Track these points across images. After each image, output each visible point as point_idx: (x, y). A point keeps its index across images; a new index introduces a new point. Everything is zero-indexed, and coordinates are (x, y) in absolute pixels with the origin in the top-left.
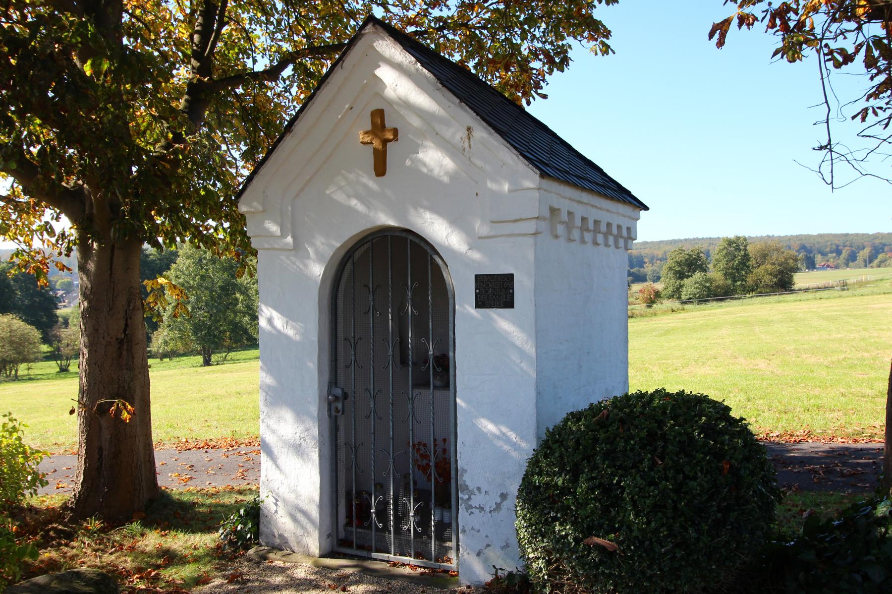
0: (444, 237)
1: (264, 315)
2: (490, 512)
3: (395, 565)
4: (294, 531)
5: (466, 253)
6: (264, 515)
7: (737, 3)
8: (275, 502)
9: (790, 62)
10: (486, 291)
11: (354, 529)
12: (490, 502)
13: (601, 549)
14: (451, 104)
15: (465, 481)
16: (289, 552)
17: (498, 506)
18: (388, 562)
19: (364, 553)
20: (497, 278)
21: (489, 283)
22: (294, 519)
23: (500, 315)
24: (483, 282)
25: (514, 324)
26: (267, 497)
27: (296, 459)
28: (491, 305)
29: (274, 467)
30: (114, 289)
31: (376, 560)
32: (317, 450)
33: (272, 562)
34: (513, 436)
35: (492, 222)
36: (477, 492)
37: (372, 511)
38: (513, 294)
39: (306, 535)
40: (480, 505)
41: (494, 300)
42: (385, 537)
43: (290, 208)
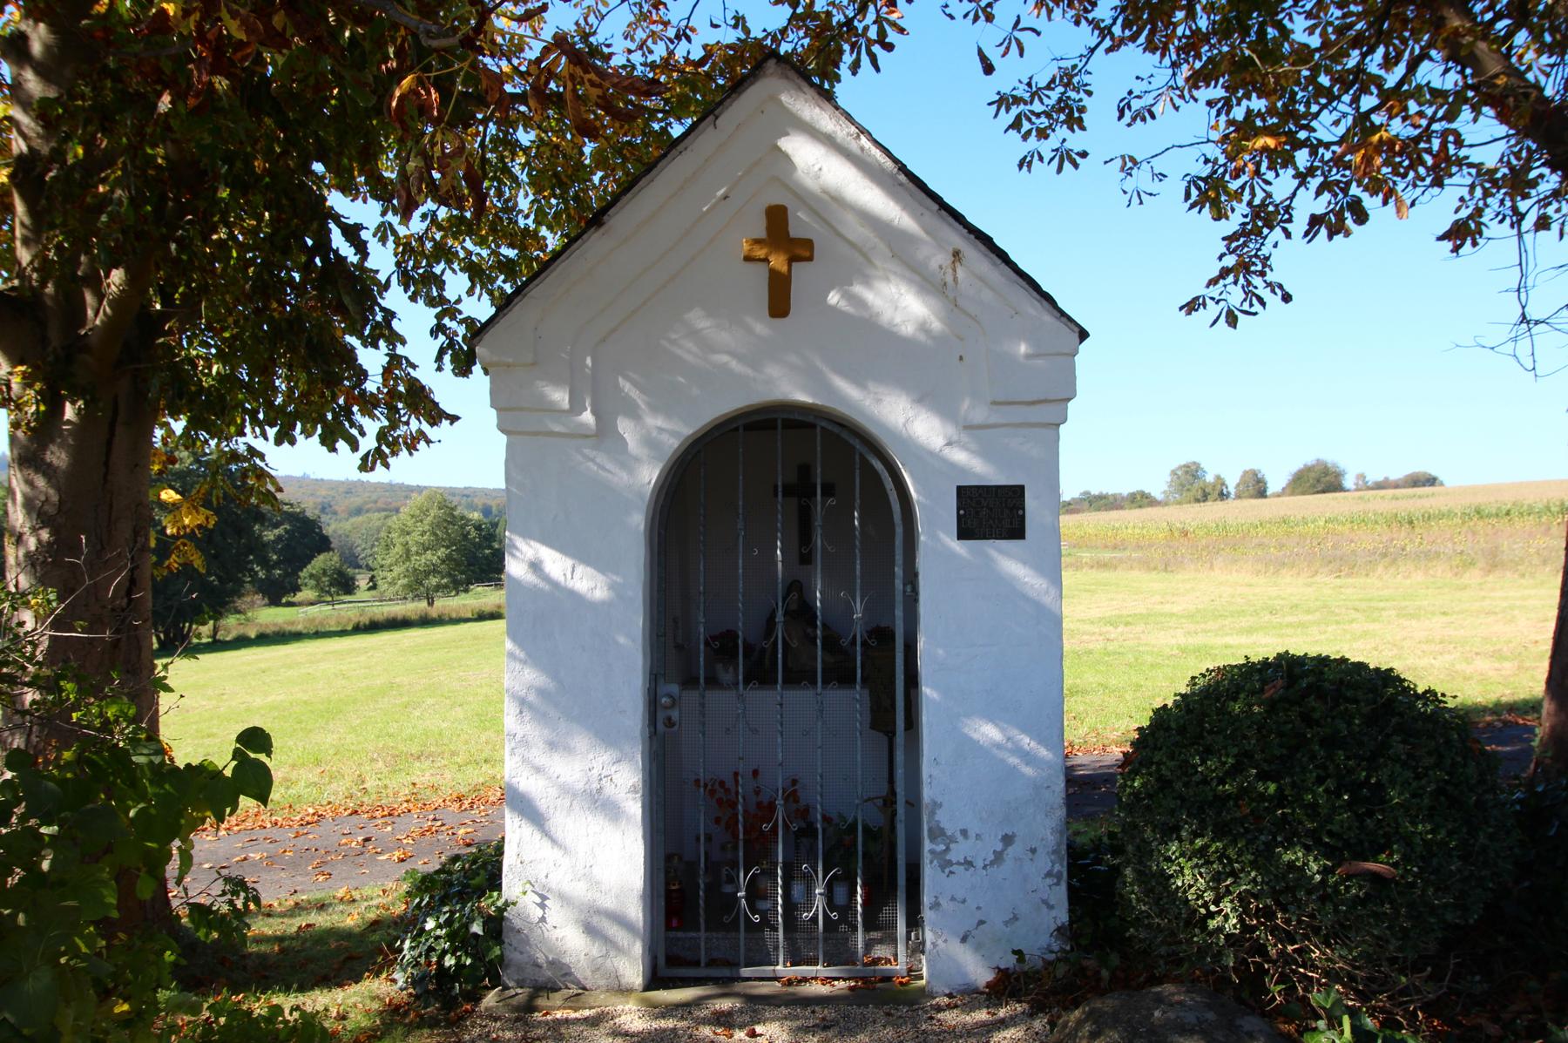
1: (518, 554)
2: (985, 867)
3: (790, 983)
6: (513, 929)
8: (538, 900)
9: (1215, 219)
11: (702, 934)
12: (982, 851)
13: (1375, 877)
14: (924, 211)
15: (938, 822)
16: (574, 990)
17: (998, 857)
18: (776, 979)
19: (726, 972)
22: (591, 930)
23: (1000, 551)
24: (971, 499)
25: (1025, 563)
26: (525, 893)
27: (590, 818)
29: (538, 835)
30: (111, 506)
31: (749, 979)
33: (547, 1014)
34: (1026, 741)
35: (994, 403)
36: (960, 838)
38: (1023, 517)
39: (612, 953)
42: (763, 939)
43: (589, 361)
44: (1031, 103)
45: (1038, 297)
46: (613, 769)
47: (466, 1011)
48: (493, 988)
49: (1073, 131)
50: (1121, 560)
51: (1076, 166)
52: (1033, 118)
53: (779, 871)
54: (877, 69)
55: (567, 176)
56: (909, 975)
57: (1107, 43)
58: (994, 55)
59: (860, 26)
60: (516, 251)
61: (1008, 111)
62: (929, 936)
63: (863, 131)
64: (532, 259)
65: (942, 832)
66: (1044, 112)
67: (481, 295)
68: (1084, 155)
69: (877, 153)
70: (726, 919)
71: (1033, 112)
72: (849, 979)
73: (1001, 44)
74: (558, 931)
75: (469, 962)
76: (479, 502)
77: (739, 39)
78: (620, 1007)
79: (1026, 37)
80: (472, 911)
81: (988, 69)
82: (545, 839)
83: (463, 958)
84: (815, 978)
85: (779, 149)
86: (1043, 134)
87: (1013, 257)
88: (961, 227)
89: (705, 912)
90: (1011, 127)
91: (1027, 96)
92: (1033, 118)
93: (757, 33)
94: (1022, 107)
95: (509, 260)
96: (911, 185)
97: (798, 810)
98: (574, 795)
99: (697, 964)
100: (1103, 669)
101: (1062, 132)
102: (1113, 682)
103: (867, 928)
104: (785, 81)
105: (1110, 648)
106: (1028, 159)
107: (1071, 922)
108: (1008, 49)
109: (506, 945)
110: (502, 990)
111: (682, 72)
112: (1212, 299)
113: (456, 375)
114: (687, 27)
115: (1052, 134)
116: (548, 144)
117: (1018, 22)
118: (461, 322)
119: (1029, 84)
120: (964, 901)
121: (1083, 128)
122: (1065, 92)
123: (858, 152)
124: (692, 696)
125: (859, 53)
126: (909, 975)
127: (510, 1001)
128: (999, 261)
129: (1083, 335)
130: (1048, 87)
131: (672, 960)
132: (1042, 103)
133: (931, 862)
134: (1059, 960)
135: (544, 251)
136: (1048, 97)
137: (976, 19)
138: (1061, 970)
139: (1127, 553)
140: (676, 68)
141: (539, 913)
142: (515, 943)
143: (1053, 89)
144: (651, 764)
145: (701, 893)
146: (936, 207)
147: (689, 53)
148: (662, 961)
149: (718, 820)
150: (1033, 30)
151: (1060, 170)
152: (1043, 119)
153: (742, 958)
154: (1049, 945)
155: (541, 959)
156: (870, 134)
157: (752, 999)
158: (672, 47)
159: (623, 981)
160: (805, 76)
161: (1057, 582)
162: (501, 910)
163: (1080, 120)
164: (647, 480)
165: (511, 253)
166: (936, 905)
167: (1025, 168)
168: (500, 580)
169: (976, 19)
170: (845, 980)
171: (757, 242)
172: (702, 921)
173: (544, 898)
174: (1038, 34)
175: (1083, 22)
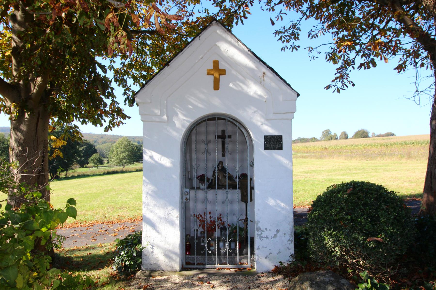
2: (272, 238)
3: (219, 269)
6: (144, 255)
8: (151, 247)
10: (270, 143)
11: (195, 256)
12: (271, 234)
14: (255, 62)
15: (259, 226)
17: (275, 236)
24: (268, 139)
26: (148, 245)
27: (165, 225)
30: (38, 141)
31: (208, 268)
32: (179, 218)
38: (282, 144)
41: (273, 146)
44: (285, 33)
46: (172, 211)
47: (132, 277)
48: (139, 270)
49: (296, 40)
50: (309, 156)
51: (297, 50)
52: (285, 37)
54: (243, 24)
57: (305, 17)
58: (274, 20)
60: (146, 73)
61: (278, 35)
63: (239, 40)
64: (150, 75)
65: (260, 229)
68: (299, 47)
70: (202, 252)
71: (285, 36)
72: (235, 268)
74: (156, 255)
75: (133, 263)
76: (137, 140)
78: (173, 276)
79: (283, 15)
81: (273, 24)
83: (131, 262)
84: (226, 268)
86: (288, 41)
87: (279, 74)
90: (279, 39)
91: (283, 31)
92: (285, 37)
94: (282, 34)
95: (145, 75)
96: (252, 55)
99: (194, 264)
101: (293, 41)
102: (306, 189)
103: (240, 255)
105: (306, 179)
107: (295, 253)
108: (278, 18)
109: (142, 259)
112: (333, 85)
114: (192, 12)
117: (281, 11)
119: (284, 28)
121: (299, 40)
123: (238, 46)
124: (193, 192)
125: (238, 19)
128: (275, 75)
129: (298, 95)
130: (289, 29)
131: (187, 263)
133: (257, 237)
134: (291, 263)
135: (153, 73)
136: (289, 31)
137: (270, 10)
138: (292, 266)
139: (310, 154)
141: (152, 250)
142: (145, 258)
143: (290, 29)
144: (182, 210)
146: (259, 61)
148: (184, 263)
150: (285, 13)
154: (289, 260)
155: (152, 263)
157: (209, 274)
158: (188, 18)
160: (224, 26)
161: (291, 161)
162: (141, 249)
163: (298, 37)
165: (145, 73)
166: (258, 249)
167: (283, 50)
169: (270, 10)
170: (234, 268)
171: (211, 70)
172: (195, 253)
173: (153, 246)
174: (286, 14)
175: (299, 11)
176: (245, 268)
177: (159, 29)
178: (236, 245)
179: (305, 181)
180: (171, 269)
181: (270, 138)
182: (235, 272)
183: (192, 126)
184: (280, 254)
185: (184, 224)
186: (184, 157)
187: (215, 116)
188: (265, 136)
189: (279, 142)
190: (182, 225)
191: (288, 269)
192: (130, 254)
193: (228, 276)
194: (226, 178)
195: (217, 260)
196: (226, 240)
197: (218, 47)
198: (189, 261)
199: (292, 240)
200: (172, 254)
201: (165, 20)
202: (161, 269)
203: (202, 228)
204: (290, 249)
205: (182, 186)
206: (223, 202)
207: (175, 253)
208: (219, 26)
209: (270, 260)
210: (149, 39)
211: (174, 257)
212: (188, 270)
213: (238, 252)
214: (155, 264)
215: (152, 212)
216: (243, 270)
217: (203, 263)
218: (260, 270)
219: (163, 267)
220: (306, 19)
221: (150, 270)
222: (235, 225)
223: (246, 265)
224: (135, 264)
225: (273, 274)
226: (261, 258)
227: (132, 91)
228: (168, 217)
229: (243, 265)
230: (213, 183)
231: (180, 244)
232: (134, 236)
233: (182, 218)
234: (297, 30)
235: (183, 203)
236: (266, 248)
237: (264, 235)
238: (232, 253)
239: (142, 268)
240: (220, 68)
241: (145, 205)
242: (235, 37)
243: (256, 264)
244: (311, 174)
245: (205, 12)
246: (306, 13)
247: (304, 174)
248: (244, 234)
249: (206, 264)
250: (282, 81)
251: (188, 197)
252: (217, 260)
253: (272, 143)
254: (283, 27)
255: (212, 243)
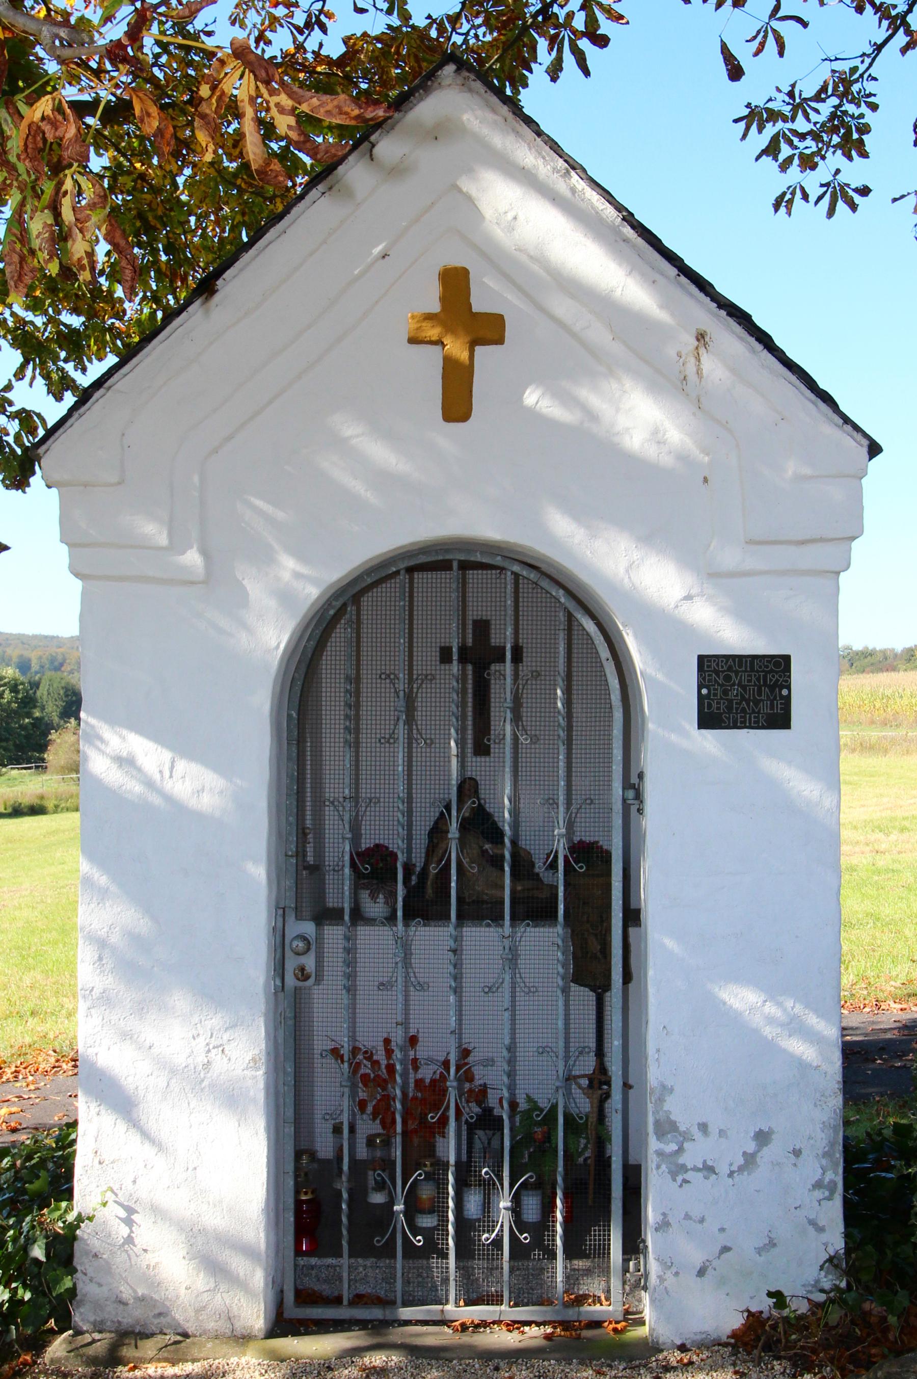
0: (622, 571)
2: (731, 1174)
3: (464, 1328)
4: (188, 1283)
5: (677, 606)
6: (87, 1253)
7: (777, 161)
8: (123, 1214)
10: (725, 692)
11: (345, 1261)
14: (658, 277)
17: (750, 1160)
19: (376, 1313)
20: (752, 663)
21: (733, 675)
24: (717, 673)
26: (105, 1204)
28: (757, 722)
29: (122, 1126)
32: (261, 1072)
33: (135, 1368)
35: (751, 542)
37: (396, 1208)
40: (705, 1161)
44: (793, 119)
45: (812, 396)
46: (226, 1037)
47: (25, 1364)
48: (61, 1331)
49: (850, 158)
50: (893, 741)
51: (853, 207)
52: (796, 141)
53: (451, 1178)
54: (587, 72)
55: (156, 217)
56: (626, 1320)
57: (901, 39)
58: (743, 53)
59: (562, 14)
60: (82, 319)
62: (654, 1267)
63: (573, 165)
64: (104, 330)
65: (673, 1126)
66: (810, 133)
67: (33, 378)
68: (864, 191)
69: (593, 196)
70: (379, 1241)
71: (795, 132)
72: (544, 1323)
73: (754, 38)
74: (149, 1255)
75: (28, 1296)
76: (14, 653)
77: (389, 27)
78: (234, 1360)
79: (787, 29)
80: (33, 1227)
81: (735, 72)
82: (132, 1131)
83: (20, 1291)
84: (498, 1322)
85: (460, 190)
86: (808, 163)
87: (779, 342)
88: (707, 300)
89: (349, 1232)
90: (765, 152)
91: (786, 110)
92: (796, 141)
93: (419, 20)
94: (780, 125)
95: (73, 331)
96: (640, 241)
97: (471, 1091)
98: (173, 1071)
99: (337, 1301)
100: (873, 892)
101: (835, 159)
102: (887, 911)
103: (570, 1254)
104: (467, 95)
105: (880, 864)
106: (788, 196)
107: (848, 1250)
108: (762, 45)
109: (78, 1275)
110: (73, 1336)
111: (311, 71)
113: (7, 487)
114: (321, 11)
115: (821, 163)
116: (129, 173)
117: (777, 8)
118: (11, 417)
119: (791, 94)
120: (702, 1221)
121: (864, 155)
122: (840, 105)
123: (568, 194)
124: (334, 934)
125: (560, 51)
126: (626, 1320)
127: (84, 1350)
128: (759, 347)
129: (874, 449)
130: (818, 98)
131: (304, 1297)
132: (808, 120)
133: (658, 1167)
134: (832, 1301)
135: (121, 319)
136: (817, 111)
138: (835, 1315)
139: (902, 732)
140: (305, 68)
141: (124, 1231)
142: (90, 1272)
143: (823, 101)
144: (276, 1029)
145: (344, 1206)
146: (673, 271)
147: (321, 45)
148: (290, 1297)
149: (362, 1105)
151: (831, 212)
152: (809, 142)
153: (399, 1295)
154: (817, 1281)
155: (126, 1293)
156: (584, 171)
157: (415, 1351)
158: (300, 38)
159: (238, 1325)
160: (484, 77)
161: (833, 781)
162: (73, 1228)
163: (861, 142)
164: (274, 643)
165: (75, 321)
167: (783, 210)
168: (43, 760)
170: (538, 1324)
171: (429, 317)
172: (345, 1244)
173: (130, 1211)
174: (805, 25)
175: (869, 9)
176: (597, 1324)
177: (261, 162)
178: (548, 1208)
179: (879, 872)
180: (222, 1326)
181: (730, 669)
182: (543, 1342)
183: (328, 603)
184: (775, 1251)
185: (290, 1100)
186: (289, 759)
187: (447, 551)
188: (701, 659)
189: (772, 688)
190: (277, 1106)
191: (813, 1329)
192: (16, 1253)
193: (510, 1365)
194: (503, 870)
195: (452, 1284)
196: (501, 1180)
197: (469, 199)
198: (311, 1283)
199: (833, 1183)
200: (227, 1252)
201: (292, 121)
202: (169, 1326)
203: (374, 1119)
204: (821, 1230)
205: (277, 908)
206: (490, 990)
207: (247, 1251)
208: (470, 90)
209: (722, 1281)
210: (98, 148)
211: (240, 1265)
212: (307, 1333)
213: (559, 1242)
214: (142, 1299)
215: (126, 1036)
216: (587, 1333)
217: (382, 1294)
218: (667, 1334)
219: (183, 1316)
220: (904, 50)
221: (116, 1332)
222: (544, 1104)
223: (598, 1307)
224: (41, 1300)
225: (735, 1353)
226: (677, 1274)
227: (18, 415)
228: (207, 1065)
229: (586, 1308)
230: (429, 891)
231: (267, 1200)
232: (29, 1158)
233: (276, 1069)
234: (858, 106)
235: (281, 995)
236: (702, 1221)
237: (693, 1156)
238: (528, 1249)
239: (77, 1318)
240: (475, 309)
241: (89, 1003)
242: (555, 147)
243: (653, 1301)
244: (906, 835)
245: (389, 12)
246: (903, 17)
247: (873, 837)
248: (586, 1147)
249: (399, 1301)
250: (793, 378)
251: (309, 962)
252: (452, 1284)
253: (735, 691)
254: (786, 89)
255: (426, 1192)
